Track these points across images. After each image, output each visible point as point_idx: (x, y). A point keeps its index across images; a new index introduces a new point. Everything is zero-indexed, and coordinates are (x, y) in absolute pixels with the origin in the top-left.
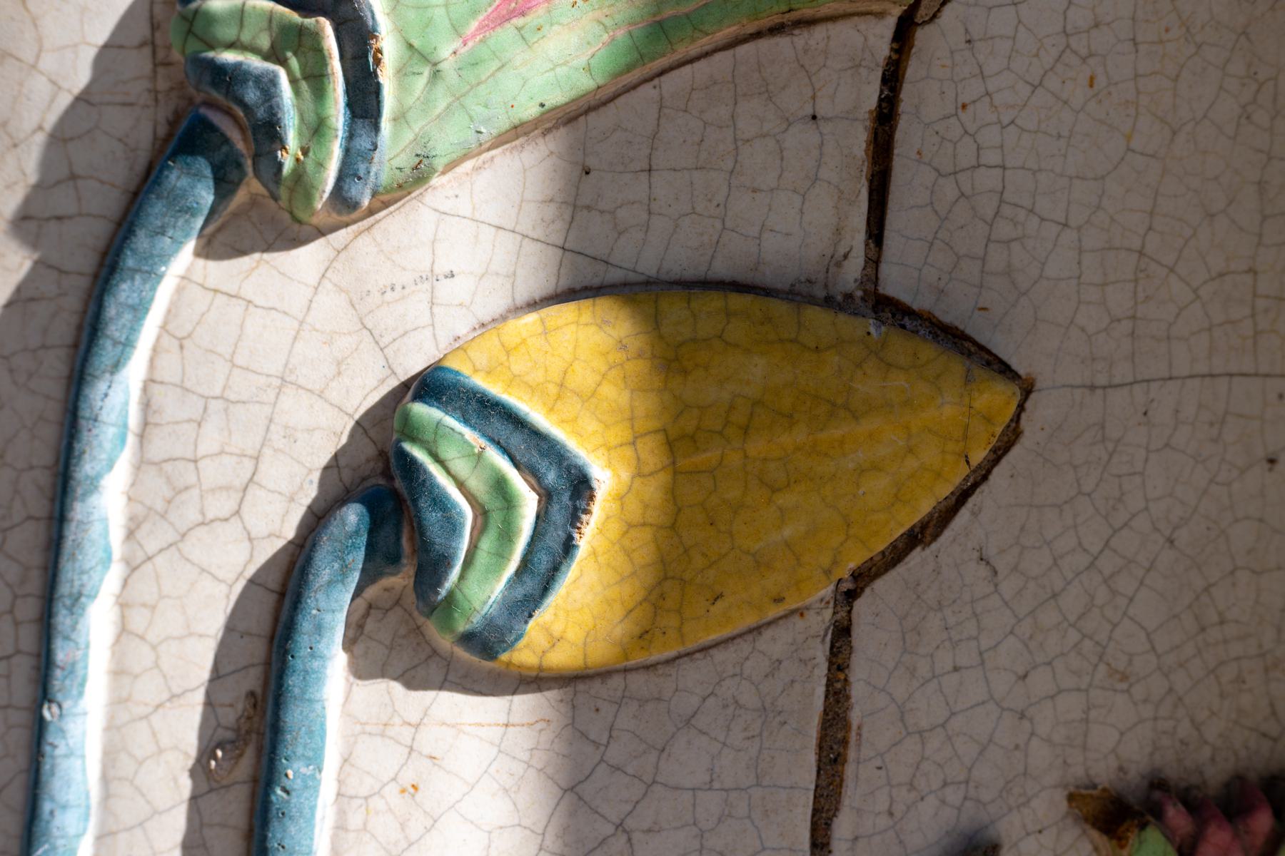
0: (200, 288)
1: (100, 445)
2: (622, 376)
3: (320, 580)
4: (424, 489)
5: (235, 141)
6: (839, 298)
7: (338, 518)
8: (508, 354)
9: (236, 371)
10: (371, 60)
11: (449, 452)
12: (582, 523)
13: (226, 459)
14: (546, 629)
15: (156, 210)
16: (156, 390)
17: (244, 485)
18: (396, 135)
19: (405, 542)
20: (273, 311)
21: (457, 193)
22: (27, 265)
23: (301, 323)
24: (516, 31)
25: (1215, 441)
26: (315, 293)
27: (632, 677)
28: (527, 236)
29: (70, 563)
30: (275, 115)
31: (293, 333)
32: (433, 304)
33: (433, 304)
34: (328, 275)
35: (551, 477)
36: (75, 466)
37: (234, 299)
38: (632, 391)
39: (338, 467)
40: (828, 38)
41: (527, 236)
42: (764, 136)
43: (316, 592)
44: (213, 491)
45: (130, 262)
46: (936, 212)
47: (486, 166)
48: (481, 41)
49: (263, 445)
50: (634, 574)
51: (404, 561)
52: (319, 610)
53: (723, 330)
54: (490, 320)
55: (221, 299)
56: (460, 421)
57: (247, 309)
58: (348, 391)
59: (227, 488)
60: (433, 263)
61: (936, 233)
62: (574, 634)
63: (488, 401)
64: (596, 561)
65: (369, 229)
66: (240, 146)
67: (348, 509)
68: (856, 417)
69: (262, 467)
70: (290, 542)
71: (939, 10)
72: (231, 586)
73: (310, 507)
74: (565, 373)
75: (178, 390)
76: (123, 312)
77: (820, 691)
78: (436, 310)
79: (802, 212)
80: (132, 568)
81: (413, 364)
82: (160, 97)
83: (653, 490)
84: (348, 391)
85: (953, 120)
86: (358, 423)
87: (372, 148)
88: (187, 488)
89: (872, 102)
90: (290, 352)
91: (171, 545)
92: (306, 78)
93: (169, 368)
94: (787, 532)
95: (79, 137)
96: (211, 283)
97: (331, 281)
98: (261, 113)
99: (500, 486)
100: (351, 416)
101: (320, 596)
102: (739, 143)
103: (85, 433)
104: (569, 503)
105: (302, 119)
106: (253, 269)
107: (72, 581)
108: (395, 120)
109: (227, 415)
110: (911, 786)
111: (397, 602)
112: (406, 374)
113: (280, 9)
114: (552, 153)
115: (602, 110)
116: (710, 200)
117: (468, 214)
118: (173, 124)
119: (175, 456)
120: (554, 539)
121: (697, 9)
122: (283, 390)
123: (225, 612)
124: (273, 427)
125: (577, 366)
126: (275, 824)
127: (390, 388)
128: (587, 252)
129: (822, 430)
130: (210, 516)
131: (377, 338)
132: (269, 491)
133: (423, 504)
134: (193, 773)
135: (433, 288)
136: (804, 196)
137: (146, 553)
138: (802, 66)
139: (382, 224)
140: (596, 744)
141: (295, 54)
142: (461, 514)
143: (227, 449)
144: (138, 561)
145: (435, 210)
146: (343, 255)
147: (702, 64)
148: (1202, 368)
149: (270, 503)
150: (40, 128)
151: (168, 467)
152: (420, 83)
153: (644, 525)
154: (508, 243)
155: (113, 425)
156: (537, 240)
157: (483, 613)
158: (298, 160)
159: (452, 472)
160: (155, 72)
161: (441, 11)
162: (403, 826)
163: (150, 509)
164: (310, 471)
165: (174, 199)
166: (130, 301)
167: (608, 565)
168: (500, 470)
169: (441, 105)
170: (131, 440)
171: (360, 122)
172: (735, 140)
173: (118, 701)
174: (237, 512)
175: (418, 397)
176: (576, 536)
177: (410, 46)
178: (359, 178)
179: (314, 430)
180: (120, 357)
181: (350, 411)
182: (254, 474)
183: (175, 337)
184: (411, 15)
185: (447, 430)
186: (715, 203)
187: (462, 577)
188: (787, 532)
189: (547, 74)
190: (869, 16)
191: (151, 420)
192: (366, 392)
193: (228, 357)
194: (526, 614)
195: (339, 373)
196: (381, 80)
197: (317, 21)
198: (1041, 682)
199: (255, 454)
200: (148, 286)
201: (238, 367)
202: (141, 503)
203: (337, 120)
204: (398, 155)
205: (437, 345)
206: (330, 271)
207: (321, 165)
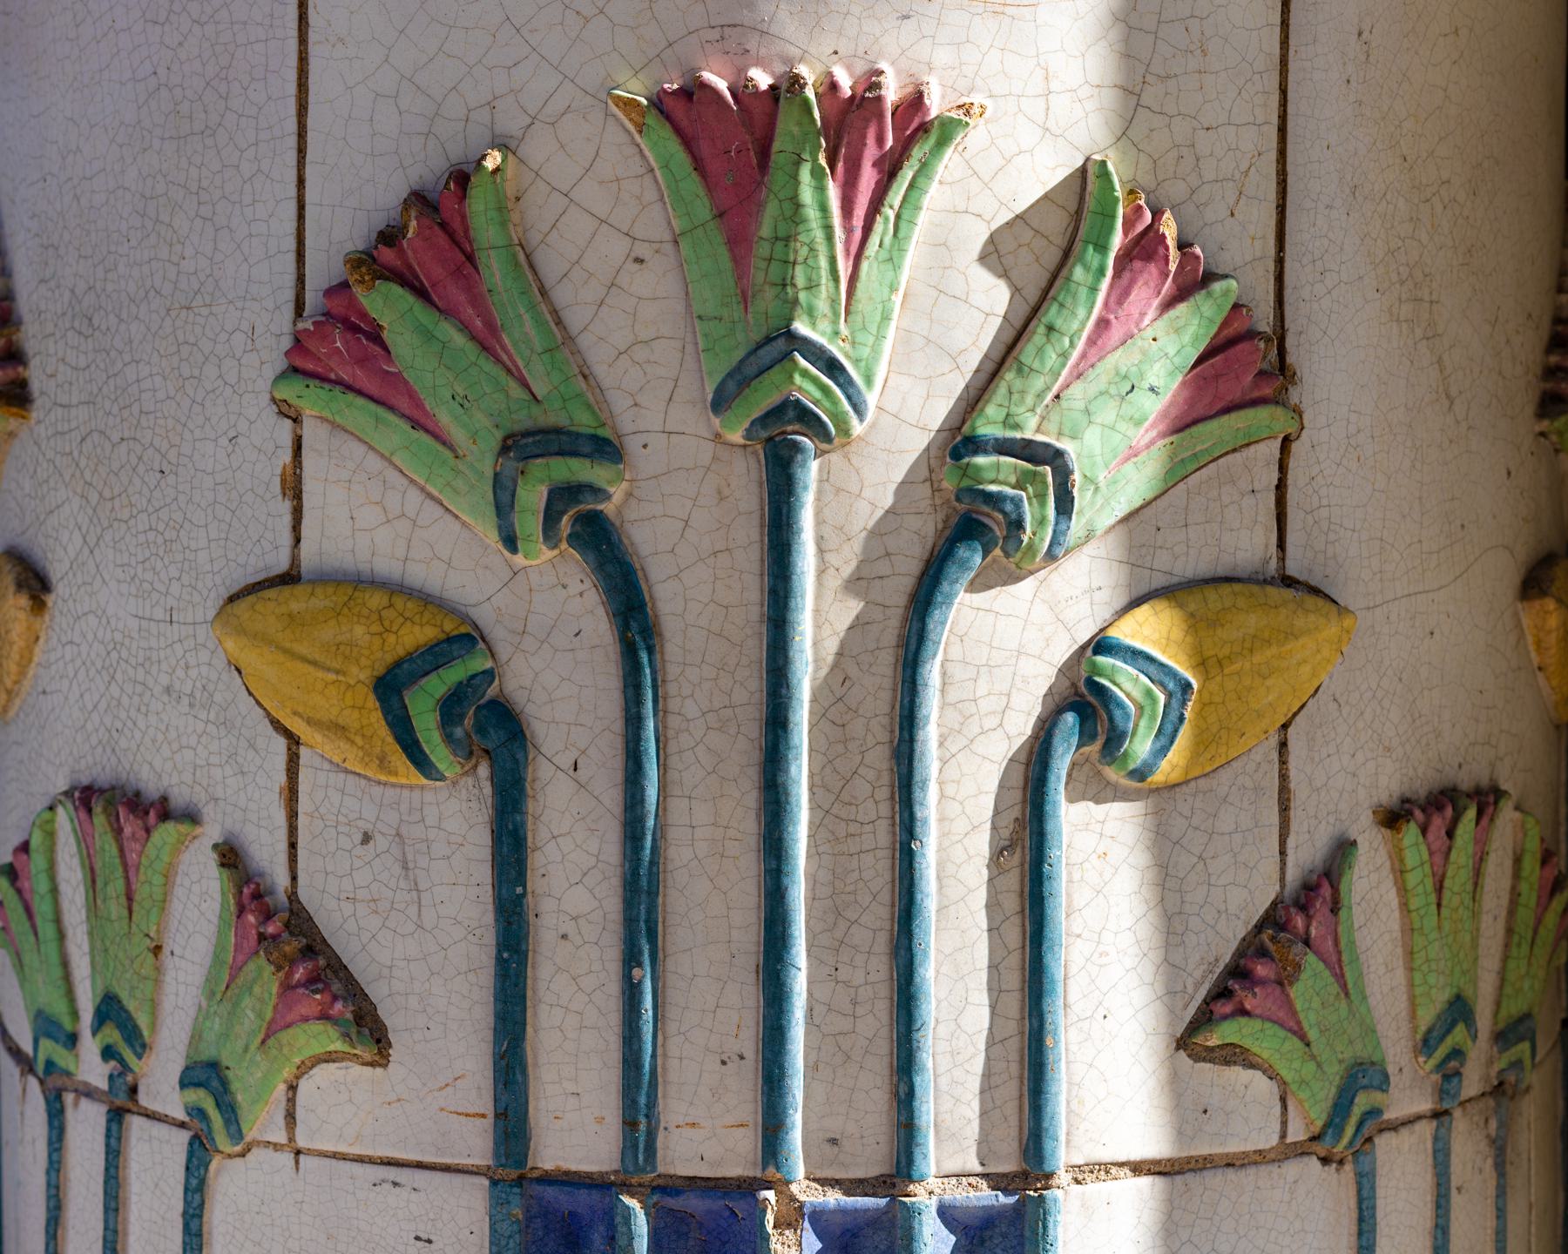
11: (1121, 679)
13: (992, 697)
15: (952, 570)
25: (1413, 627)
27: (1199, 781)
35: (1171, 685)
45: (939, 599)
55: (981, 613)
66: (998, 533)
81: (1084, 636)
94: (1270, 698)
96: (975, 605)
98: (1014, 516)
99: (1149, 694)
110: (1316, 818)
120: (1173, 716)
126: (1046, 883)
134: (988, 866)
140: (1186, 818)
148: (1406, 592)
151: (960, 706)
162: (1101, 875)
173: (943, 835)
175: (1097, 652)
198: (1360, 757)
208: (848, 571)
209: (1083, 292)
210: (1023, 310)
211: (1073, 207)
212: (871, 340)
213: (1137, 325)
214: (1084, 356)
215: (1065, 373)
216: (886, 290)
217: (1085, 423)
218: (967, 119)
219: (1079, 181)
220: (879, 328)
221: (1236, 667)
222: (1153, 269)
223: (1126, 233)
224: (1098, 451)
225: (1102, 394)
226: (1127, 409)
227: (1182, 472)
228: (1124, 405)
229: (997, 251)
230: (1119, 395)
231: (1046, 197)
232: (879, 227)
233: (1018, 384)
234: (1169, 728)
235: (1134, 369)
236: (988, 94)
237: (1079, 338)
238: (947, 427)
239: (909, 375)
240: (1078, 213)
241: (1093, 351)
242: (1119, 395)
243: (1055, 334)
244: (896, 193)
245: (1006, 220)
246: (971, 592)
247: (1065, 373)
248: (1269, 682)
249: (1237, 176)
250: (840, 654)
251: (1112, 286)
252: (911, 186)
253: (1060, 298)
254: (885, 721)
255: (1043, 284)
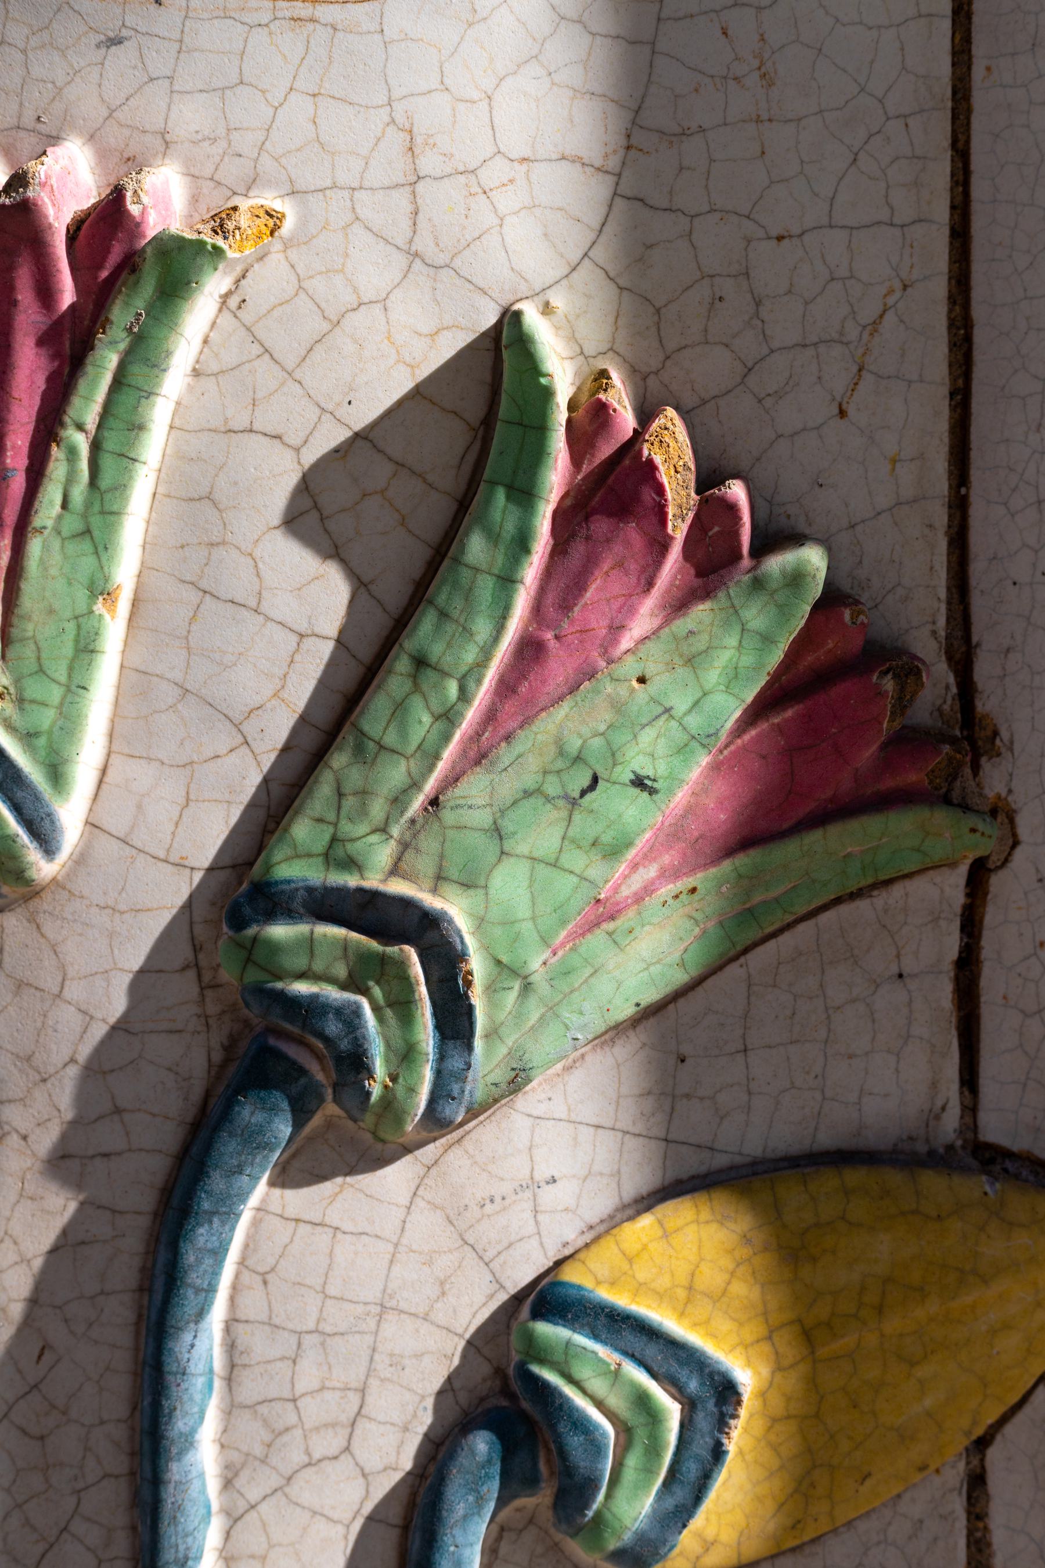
0: (279, 1218)
1: (191, 1399)
2: (750, 1271)
3: (455, 1515)
4: (562, 1414)
5: (315, 1073)
6: (941, 1150)
7: (466, 1448)
8: (630, 1261)
9: (329, 1302)
10: (460, 982)
11: (584, 1372)
12: (730, 1428)
13: (328, 1395)
14: (699, 1535)
15: (228, 1147)
16: (240, 1328)
17: (352, 1420)
18: (489, 1051)
19: (543, 1467)
20: (364, 1237)
21: (550, 1095)
22: (73, 1206)
23: (396, 1245)
24: (607, 936)
26: (408, 1213)
28: (628, 1133)
29: (172, 1528)
30: (361, 1046)
31: (389, 1256)
32: (536, 1212)
33: (536, 1212)
34: (420, 1192)
35: (693, 1386)
36: (166, 1424)
37: (319, 1227)
38: (763, 1285)
39: (453, 1390)
40: (907, 895)
41: (628, 1133)
42: (854, 1001)
43: (451, 1528)
44: (317, 1429)
45: (206, 1205)
46: (1026, 1053)
47: (577, 1065)
48: (571, 949)
49: (368, 1376)
50: (782, 1467)
51: (543, 1485)
52: (457, 1546)
53: (845, 1210)
54: (598, 1221)
55: (304, 1228)
56: (590, 1338)
57: (334, 1236)
58: (455, 1311)
59: (333, 1425)
60: (532, 1170)
61: (1028, 1073)
62: (728, 1536)
63: (618, 1315)
64: (744, 1460)
65: (459, 1141)
66: (320, 1077)
67: (475, 1437)
68: (985, 1281)
69: (370, 1400)
70: (409, 1473)
71: (1010, 854)
72: (348, 1527)
73: (426, 1435)
74: (693, 1275)
75: (267, 1328)
76: (203, 1258)
77: (962, 1543)
78: (540, 1217)
79: (897, 1070)
80: (234, 1519)
81: (521, 1275)
82: (211, 1021)
83: (792, 1382)
84: (455, 1311)
85: (1033, 959)
86: (469, 1343)
87: (465, 1067)
88: (287, 1429)
89: (953, 953)
90: (388, 1276)
91: (276, 1490)
92: (390, 1005)
93: (253, 1305)
94: (928, 1402)
95: (121, 1068)
96: (290, 1212)
97: (423, 1199)
99: (642, 1401)
100: (461, 1336)
101: (457, 1532)
102: (831, 1011)
103: (174, 1389)
104: (715, 1410)
105: (388, 1045)
106: (337, 1194)
107: (177, 1546)
108: (486, 1036)
109: (325, 1349)
111: (531, 1521)
112: (515, 1287)
113: (354, 935)
114: (644, 1044)
115: (691, 995)
116: (808, 1073)
117: (564, 1116)
118: (230, 1047)
119: (270, 1396)
120: (701, 1446)
121: (786, 892)
122: (384, 1316)
123: (345, 1555)
124: (377, 1357)
125: (705, 1268)
127: (500, 1303)
128: (691, 1141)
129: (953, 1298)
130: (317, 1455)
131: (481, 1253)
132: (380, 1423)
133: (562, 1428)
135: (535, 1196)
136: (898, 1055)
137: (248, 1501)
138: (884, 926)
139: (473, 1135)
141: (378, 983)
142: (605, 1435)
143: (328, 1384)
144: (241, 1511)
145: (529, 1115)
146: (434, 1171)
147: (786, 938)
149: (383, 1435)
150: (73, 1060)
151: (263, 1409)
152: (511, 998)
153: (788, 1417)
154: (608, 1141)
155: (201, 1375)
156: (639, 1135)
157: (634, 1529)
158: (386, 1087)
159: (589, 1391)
160: (202, 995)
161: (529, 925)
163: (247, 1455)
164: (423, 1398)
165: (250, 1137)
166: (209, 1245)
167: (756, 1462)
168: (640, 1386)
169: (534, 1017)
170: (217, 1384)
171: (450, 1044)
172: (827, 1009)
174: (347, 1449)
176: (725, 1441)
177: (499, 962)
178: (453, 1099)
179: (423, 1354)
180: (204, 1304)
181: (460, 1331)
182: (361, 1407)
183: (257, 1273)
184: (498, 931)
185: (579, 1349)
186: (813, 1075)
187: (609, 1496)
188: (928, 1402)
189: (641, 975)
190: (943, 868)
191: (237, 1360)
192: (474, 1310)
193: (319, 1288)
194: (680, 1525)
195: (443, 1293)
196: (473, 1002)
197: (401, 949)
199: (360, 1386)
200: (227, 1228)
201: (330, 1297)
202: (237, 1449)
203: (428, 1045)
204: (492, 1071)
205: (545, 1254)
206: (422, 1188)
207: (412, 1090)
208: (46, 1140)
209: (486, 587)
210: (378, 624)
211: (475, 412)
212: (56, 694)
213: (605, 652)
214: (490, 717)
215: (449, 753)
216: (81, 594)
217: (492, 857)
218: (220, 242)
219: (488, 359)
220: (71, 669)
221: (848, 1341)
222: (632, 533)
223: (577, 458)
224: (523, 911)
225: (527, 794)
226: (583, 825)
227: (753, 934)
228: (577, 817)
229: (316, 506)
230: (566, 797)
231: (418, 393)
232: (57, 469)
233: (355, 777)
234: (691, 1470)
235: (597, 742)
236: (287, 188)
237: (479, 682)
238: (227, 861)
239: (149, 759)
240: (488, 421)
241: (510, 706)
242: (566, 797)
243: (429, 672)
244: (88, 399)
245: (333, 444)
246: (284, 1185)
247: (449, 753)
248: (923, 1371)
249: (852, 332)
250: (33, 1301)
251: (548, 574)
252: (118, 382)
253: (441, 599)
254: (120, 1433)
255: (416, 571)
